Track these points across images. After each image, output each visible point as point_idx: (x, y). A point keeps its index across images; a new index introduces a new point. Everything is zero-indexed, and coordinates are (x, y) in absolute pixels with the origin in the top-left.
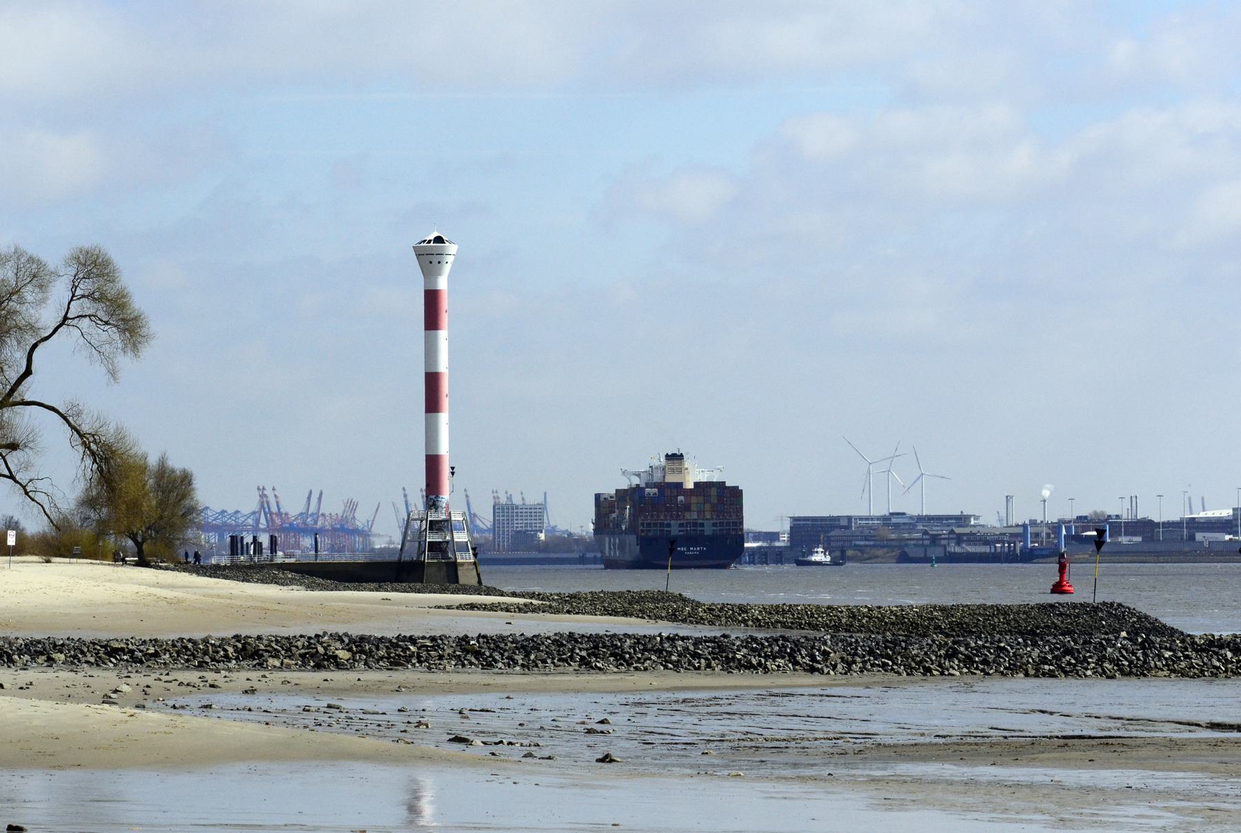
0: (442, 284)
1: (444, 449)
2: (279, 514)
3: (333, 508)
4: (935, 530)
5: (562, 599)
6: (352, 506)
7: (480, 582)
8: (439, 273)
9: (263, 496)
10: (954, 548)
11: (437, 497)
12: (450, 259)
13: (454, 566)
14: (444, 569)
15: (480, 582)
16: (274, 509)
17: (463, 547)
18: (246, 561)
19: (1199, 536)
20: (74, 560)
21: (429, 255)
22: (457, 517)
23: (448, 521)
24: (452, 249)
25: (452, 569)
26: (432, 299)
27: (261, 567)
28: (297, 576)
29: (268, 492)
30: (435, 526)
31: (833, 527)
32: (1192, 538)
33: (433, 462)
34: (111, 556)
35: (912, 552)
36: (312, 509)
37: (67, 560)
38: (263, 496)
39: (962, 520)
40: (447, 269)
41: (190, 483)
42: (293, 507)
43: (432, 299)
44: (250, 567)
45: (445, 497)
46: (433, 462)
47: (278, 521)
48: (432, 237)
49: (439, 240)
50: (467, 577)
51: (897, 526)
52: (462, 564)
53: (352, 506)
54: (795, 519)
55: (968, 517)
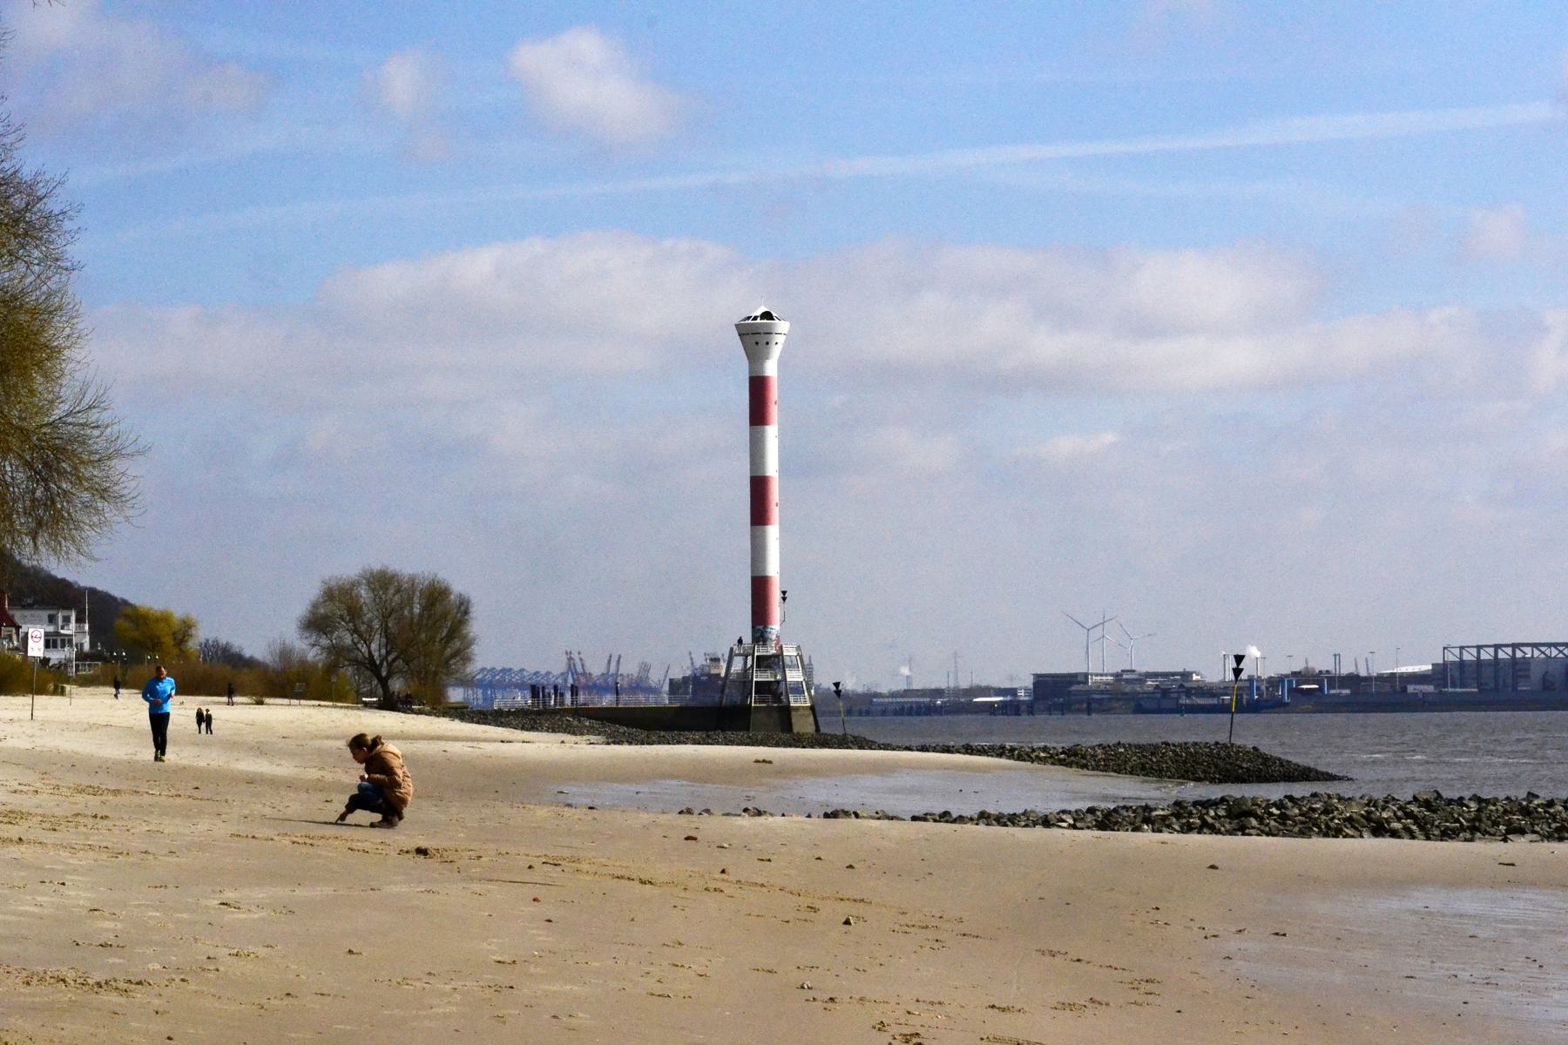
0: (771, 369)
1: (773, 569)
2: (584, 674)
3: (629, 669)
4: (1167, 684)
5: (992, 748)
6: (645, 668)
7: (818, 730)
8: (766, 356)
9: (570, 659)
10: (1184, 701)
11: (766, 627)
12: (780, 339)
13: (786, 711)
14: (776, 715)
15: (818, 730)
16: (580, 670)
17: (797, 689)
18: (545, 709)
19: (1411, 689)
20: (294, 702)
21: (754, 336)
22: (789, 652)
23: (779, 656)
24: (782, 326)
25: (785, 714)
26: (758, 388)
27: (554, 712)
28: (596, 724)
29: (575, 656)
30: (764, 662)
31: (1071, 683)
32: (1404, 689)
33: (760, 586)
34: (353, 694)
35: (1146, 704)
36: (613, 669)
37: (286, 701)
38: (570, 659)
39: (1186, 675)
40: (776, 351)
41: (466, 612)
42: (596, 669)
43: (758, 388)
44: (539, 713)
45: (775, 628)
46: (760, 586)
47: (583, 680)
48: (758, 313)
49: (767, 315)
50: (803, 725)
51: (1127, 681)
52: (797, 709)
53: (645, 668)
54: (1037, 676)
55: (1190, 674)
